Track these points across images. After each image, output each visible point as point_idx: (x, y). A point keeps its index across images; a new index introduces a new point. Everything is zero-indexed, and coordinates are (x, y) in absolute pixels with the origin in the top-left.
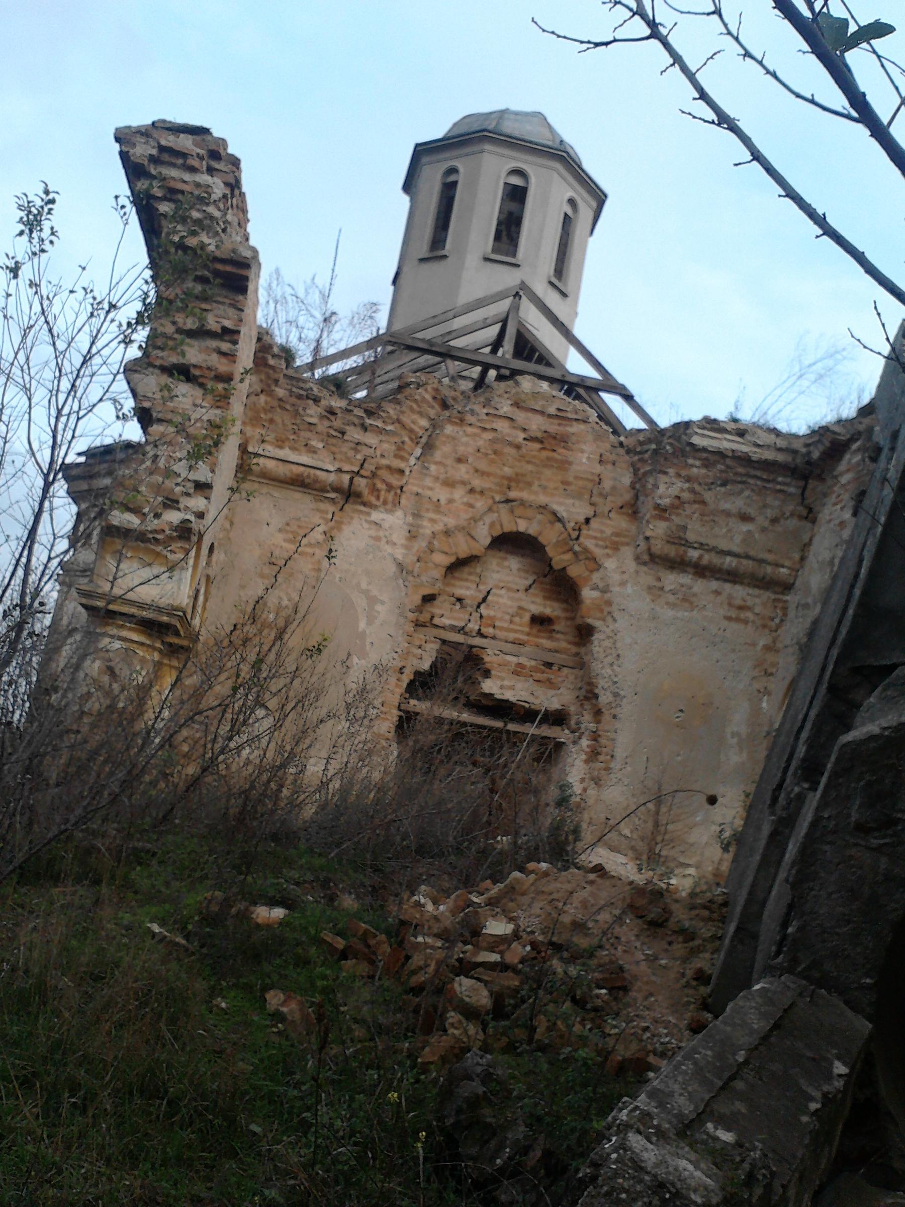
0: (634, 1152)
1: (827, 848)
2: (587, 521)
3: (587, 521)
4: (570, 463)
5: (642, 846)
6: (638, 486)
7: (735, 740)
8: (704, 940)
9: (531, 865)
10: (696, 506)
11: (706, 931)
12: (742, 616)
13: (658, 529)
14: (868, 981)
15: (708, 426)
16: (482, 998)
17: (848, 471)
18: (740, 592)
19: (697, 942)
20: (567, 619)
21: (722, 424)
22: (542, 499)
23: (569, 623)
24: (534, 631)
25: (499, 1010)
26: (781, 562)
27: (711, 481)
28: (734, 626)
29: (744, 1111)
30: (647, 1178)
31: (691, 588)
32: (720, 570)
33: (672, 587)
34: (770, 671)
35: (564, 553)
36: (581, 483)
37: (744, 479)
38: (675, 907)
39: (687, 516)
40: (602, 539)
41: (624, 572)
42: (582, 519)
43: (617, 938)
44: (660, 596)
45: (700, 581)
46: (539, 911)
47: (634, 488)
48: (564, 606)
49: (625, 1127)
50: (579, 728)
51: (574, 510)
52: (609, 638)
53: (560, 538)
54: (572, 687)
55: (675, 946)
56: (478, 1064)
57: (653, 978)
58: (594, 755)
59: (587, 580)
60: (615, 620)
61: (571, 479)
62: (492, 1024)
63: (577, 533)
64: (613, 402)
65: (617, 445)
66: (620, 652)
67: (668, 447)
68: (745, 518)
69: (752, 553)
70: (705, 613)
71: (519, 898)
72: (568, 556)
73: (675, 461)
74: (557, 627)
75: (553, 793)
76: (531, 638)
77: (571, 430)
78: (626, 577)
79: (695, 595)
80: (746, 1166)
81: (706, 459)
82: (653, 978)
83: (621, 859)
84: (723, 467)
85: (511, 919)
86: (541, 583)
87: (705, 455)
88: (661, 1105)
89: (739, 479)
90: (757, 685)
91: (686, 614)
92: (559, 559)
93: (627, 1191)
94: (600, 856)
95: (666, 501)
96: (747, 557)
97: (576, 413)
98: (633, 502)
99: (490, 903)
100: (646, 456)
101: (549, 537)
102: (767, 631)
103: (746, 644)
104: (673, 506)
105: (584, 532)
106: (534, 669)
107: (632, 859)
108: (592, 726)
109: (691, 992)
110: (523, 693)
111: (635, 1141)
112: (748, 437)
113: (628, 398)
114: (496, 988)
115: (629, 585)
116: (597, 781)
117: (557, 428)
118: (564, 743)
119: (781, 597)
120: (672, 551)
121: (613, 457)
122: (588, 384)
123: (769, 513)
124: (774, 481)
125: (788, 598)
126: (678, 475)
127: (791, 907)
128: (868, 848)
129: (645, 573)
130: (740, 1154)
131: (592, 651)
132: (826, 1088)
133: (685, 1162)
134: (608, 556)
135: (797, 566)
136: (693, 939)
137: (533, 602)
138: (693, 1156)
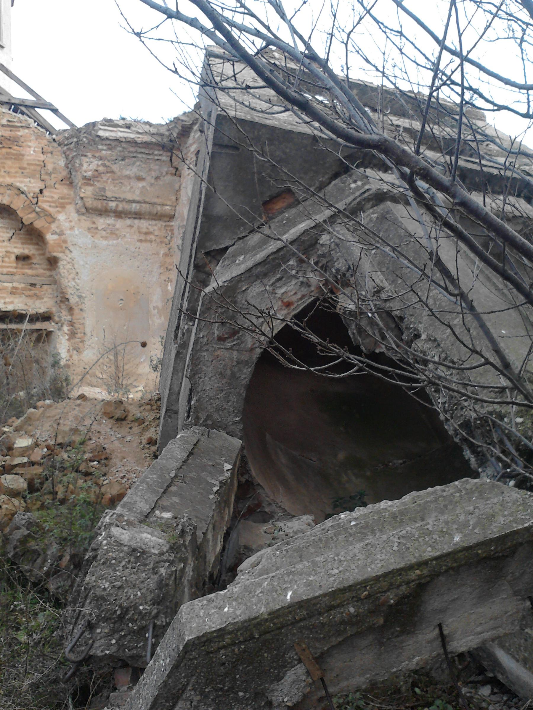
0: (116, 537)
1: (205, 354)
2: (41, 191)
3: (41, 191)
4: (23, 155)
5: (112, 382)
6: (70, 166)
7: (156, 311)
8: (150, 422)
9: (40, 403)
10: (109, 175)
11: (150, 417)
12: (148, 238)
13: (88, 191)
14: (237, 419)
15: (107, 124)
16: (21, 484)
17: (194, 143)
18: (144, 224)
19: (146, 424)
20: (40, 255)
21: (115, 122)
22: (8, 180)
23: (42, 257)
24: (20, 265)
25: (32, 488)
26: (165, 203)
27: (115, 158)
28: (144, 244)
29: (177, 501)
30: (126, 548)
31: (114, 226)
32: (130, 213)
33: (103, 226)
34: (169, 268)
35: (29, 213)
36: (32, 167)
37: (135, 155)
38: (130, 408)
39: (104, 182)
40: (53, 202)
41: (71, 221)
42: (37, 190)
43: (99, 432)
44: (96, 233)
45: (119, 220)
46: (49, 428)
47: (67, 168)
48: (36, 247)
49: (108, 526)
50: (61, 320)
51: (31, 185)
52: (69, 263)
53: (25, 204)
54: (51, 296)
55: (133, 429)
56: (22, 519)
57: (124, 449)
58: (72, 335)
59: (49, 228)
60: (71, 252)
61: (25, 166)
62: (29, 496)
63: (36, 199)
64: (46, 114)
65: (52, 140)
66: (78, 271)
67: (84, 140)
68: (140, 179)
69: (147, 200)
70: (126, 240)
71: (34, 423)
72: (33, 215)
73: (90, 147)
74: (34, 261)
75: (50, 360)
76: (19, 270)
77: (20, 134)
78: (73, 224)
79: (118, 229)
80: (180, 527)
81: (110, 144)
82: (124, 449)
83: (98, 390)
84: (121, 149)
85: (31, 436)
86: (19, 234)
87: (108, 142)
88: (130, 510)
89: (132, 155)
90: (163, 277)
91: (114, 242)
92: (27, 218)
93: (115, 559)
94: (87, 390)
95: (89, 174)
96: (145, 202)
97: (21, 122)
98: (68, 176)
99: (16, 430)
100: (72, 146)
101: (17, 204)
102: (164, 245)
103: (153, 254)
104: (94, 176)
105: (40, 198)
106: (23, 289)
107: (105, 389)
108: (69, 318)
109: (146, 451)
110: (20, 305)
111: (115, 531)
112: (133, 128)
113: (55, 111)
114: (29, 476)
115: (76, 229)
116: (77, 350)
117: (10, 133)
118: (52, 331)
119: (168, 223)
120: (98, 204)
121: (50, 149)
122: (27, 104)
123: (153, 174)
124: (153, 154)
125: (172, 224)
126: (94, 157)
127: (191, 390)
128: (226, 349)
129: (85, 220)
130: (176, 522)
131: (59, 273)
132: (221, 478)
133: (145, 534)
134: (59, 212)
135: (175, 204)
136: (144, 423)
137: (15, 247)
138: (150, 530)
